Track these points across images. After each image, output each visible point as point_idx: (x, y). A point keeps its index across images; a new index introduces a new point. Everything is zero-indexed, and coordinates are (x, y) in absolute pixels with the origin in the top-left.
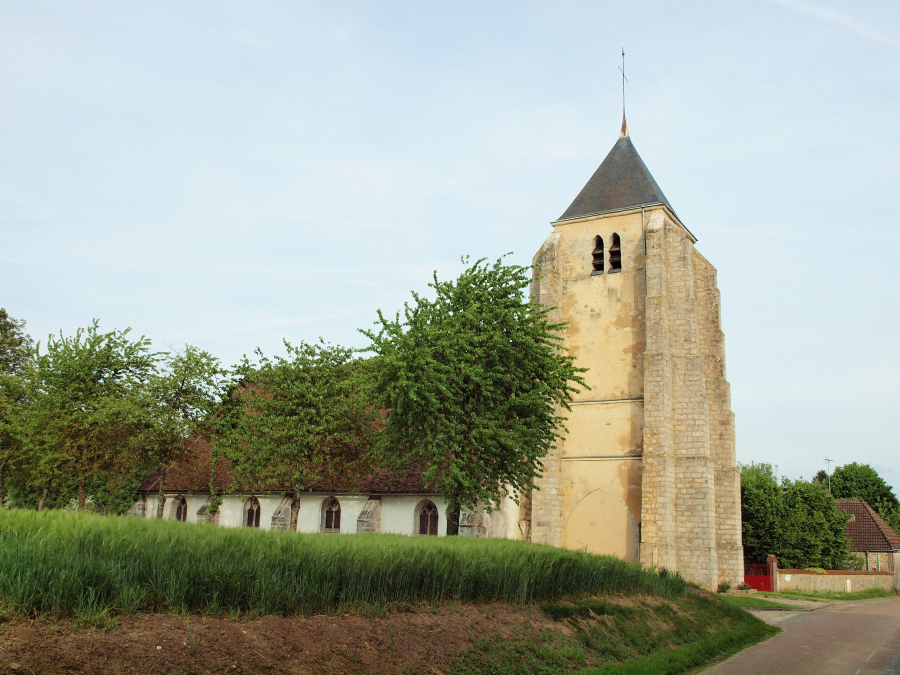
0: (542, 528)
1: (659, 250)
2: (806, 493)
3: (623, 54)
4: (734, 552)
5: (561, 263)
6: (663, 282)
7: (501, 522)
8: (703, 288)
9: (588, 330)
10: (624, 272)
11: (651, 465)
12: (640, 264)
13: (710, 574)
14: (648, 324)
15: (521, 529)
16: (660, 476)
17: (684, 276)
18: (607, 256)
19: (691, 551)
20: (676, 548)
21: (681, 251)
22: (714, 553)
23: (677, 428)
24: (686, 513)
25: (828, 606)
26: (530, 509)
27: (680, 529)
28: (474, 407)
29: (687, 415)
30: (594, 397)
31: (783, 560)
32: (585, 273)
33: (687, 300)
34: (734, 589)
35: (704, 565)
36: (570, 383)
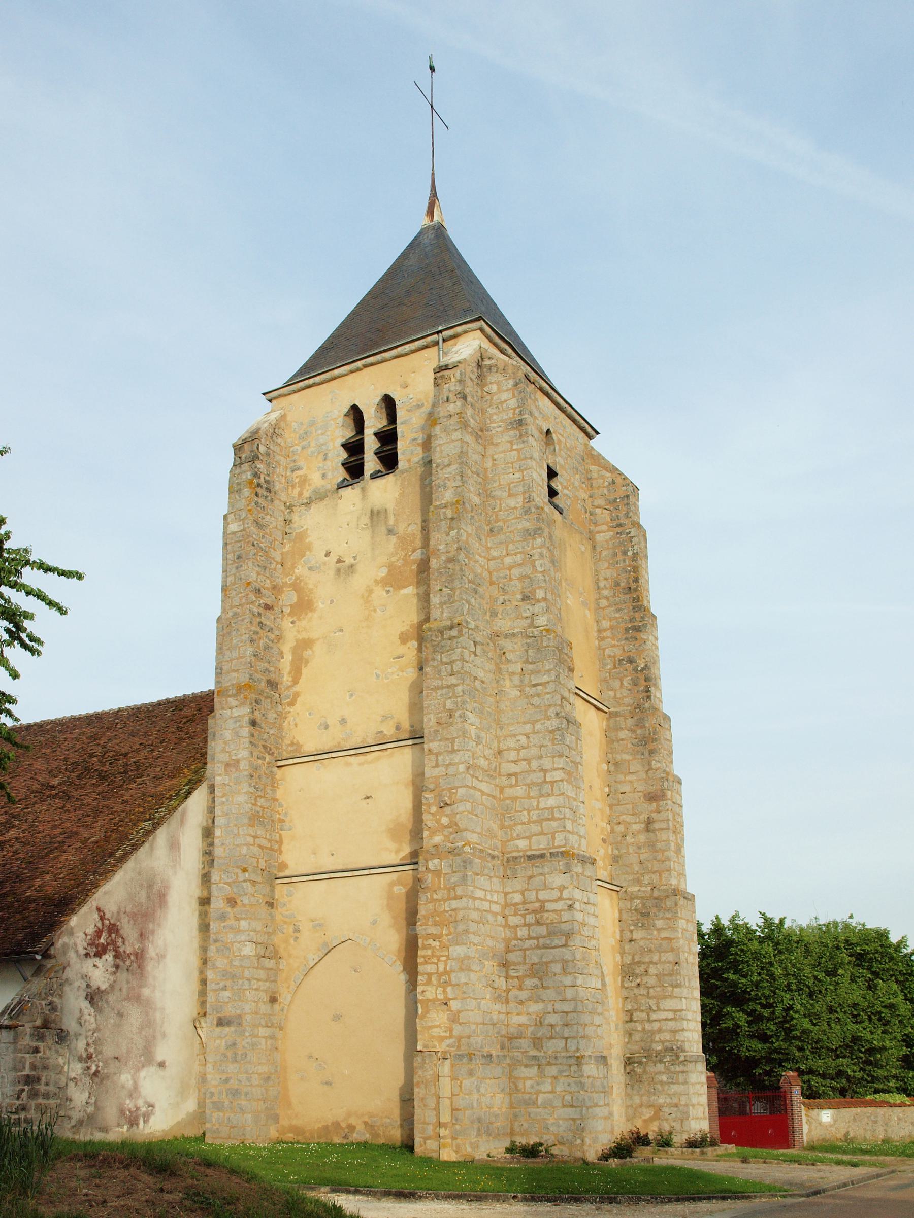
0: (227, 1030)
2: (858, 945)
3: (432, 69)
9: (332, 602)
10: (403, 472)
11: (437, 873)
14: (434, 563)
15: (199, 1036)
16: (455, 898)
17: (519, 459)
18: (371, 444)
19: (539, 1066)
21: (514, 409)
23: (509, 792)
24: (529, 982)
25: (878, 1176)
29: (528, 761)
30: (342, 743)
31: (816, 1081)
32: (329, 487)
33: (527, 511)
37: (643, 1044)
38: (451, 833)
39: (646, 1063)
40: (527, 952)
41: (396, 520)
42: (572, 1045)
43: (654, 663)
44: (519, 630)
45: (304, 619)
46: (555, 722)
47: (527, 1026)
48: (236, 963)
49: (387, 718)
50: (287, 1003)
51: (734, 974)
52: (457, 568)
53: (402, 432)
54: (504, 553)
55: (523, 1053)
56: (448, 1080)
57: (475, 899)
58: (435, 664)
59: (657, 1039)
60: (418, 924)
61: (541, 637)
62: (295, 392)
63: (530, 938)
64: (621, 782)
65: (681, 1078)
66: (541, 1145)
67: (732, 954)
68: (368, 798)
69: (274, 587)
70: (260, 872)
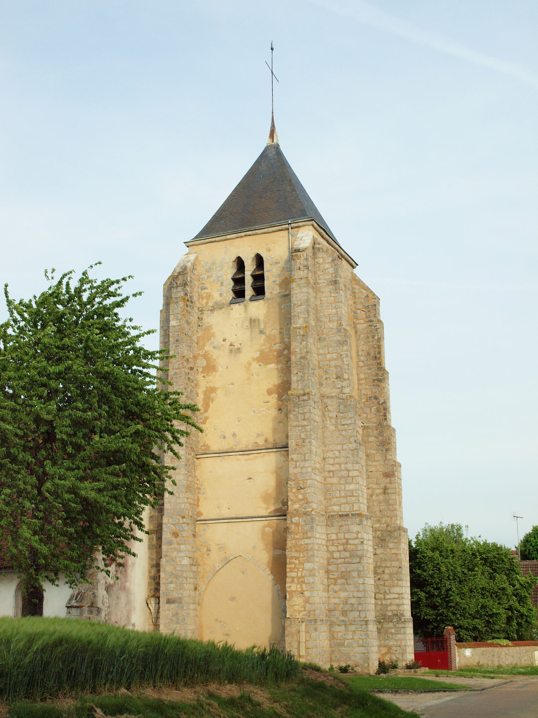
0: (172, 606)
1: (306, 272)
3: (272, 49)
4: (400, 626)
5: (195, 289)
6: (310, 309)
7: (123, 600)
8: (363, 319)
9: (227, 367)
10: (268, 299)
11: (297, 525)
12: (286, 290)
13: (368, 653)
14: (293, 358)
16: (307, 538)
17: (335, 302)
18: (249, 281)
19: (345, 625)
20: (329, 623)
21: (332, 274)
22: (373, 628)
23: (329, 480)
24: (340, 581)
25: (506, 683)
26: (158, 584)
27: (333, 601)
28: (49, 454)
29: (340, 465)
30: (234, 447)
31: (463, 633)
32: (224, 301)
33: (339, 331)
34: (401, 669)
35: (361, 642)
36: (177, 424)
37: (381, 612)
38: (304, 503)
39: (383, 622)
40: (339, 566)
41: (265, 327)
42: (363, 615)
43: (388, 399)
44: (335, 394)
45: (211, 375)
46: (354, 445)
47: (339, 604)
48: (179, 569)
49: (260, 435)
50: (203, 590)
51: (419, 569)
52: (306, 362)
53: (268, 276)
54: (327, 352)
55: (336, 618)
56: (304, 633)
57: (316, 538)
58: (295, 413)
59: (389, 609)
60: (287, 551)
61: (347, 400)
62: (203, 244)
63: (340, 558)
64: (370, 465)
65: (402, 630)
66: (349, 666)
67: (418, 558)
68: (250, 479)
69: (194, 357)
70: (190, 518)
